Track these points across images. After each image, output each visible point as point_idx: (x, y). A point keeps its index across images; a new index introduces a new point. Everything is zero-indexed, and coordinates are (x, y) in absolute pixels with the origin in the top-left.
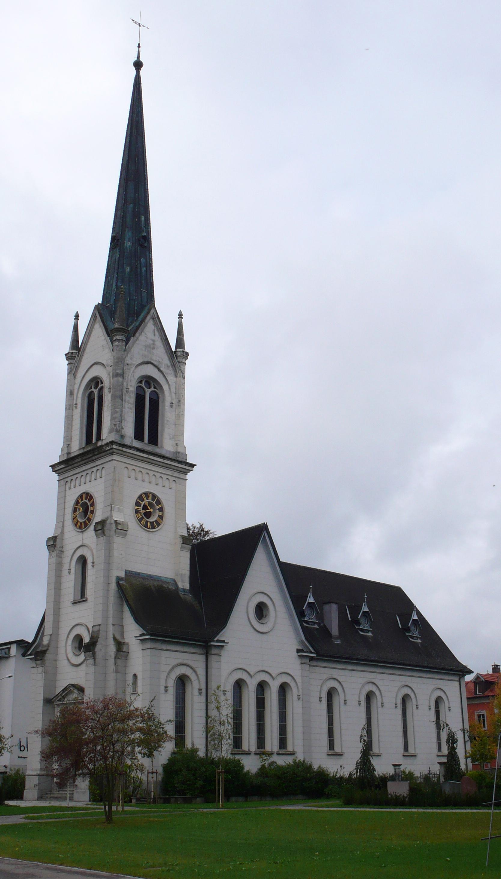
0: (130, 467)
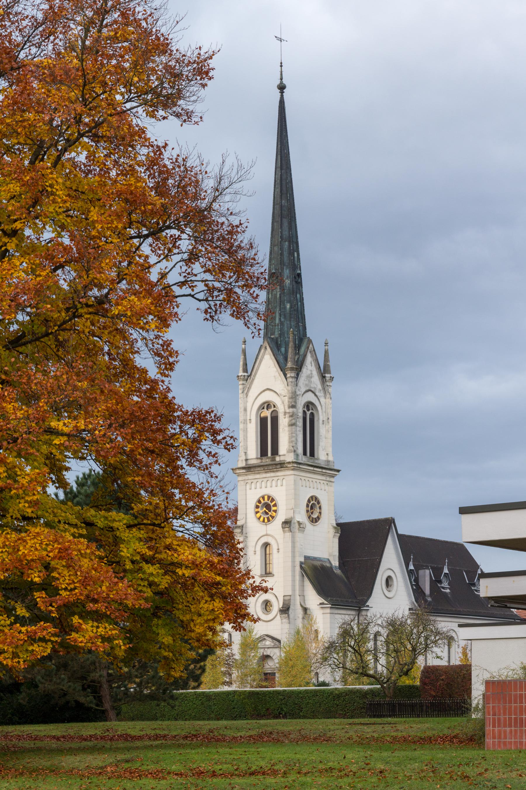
0: (303, 478)
